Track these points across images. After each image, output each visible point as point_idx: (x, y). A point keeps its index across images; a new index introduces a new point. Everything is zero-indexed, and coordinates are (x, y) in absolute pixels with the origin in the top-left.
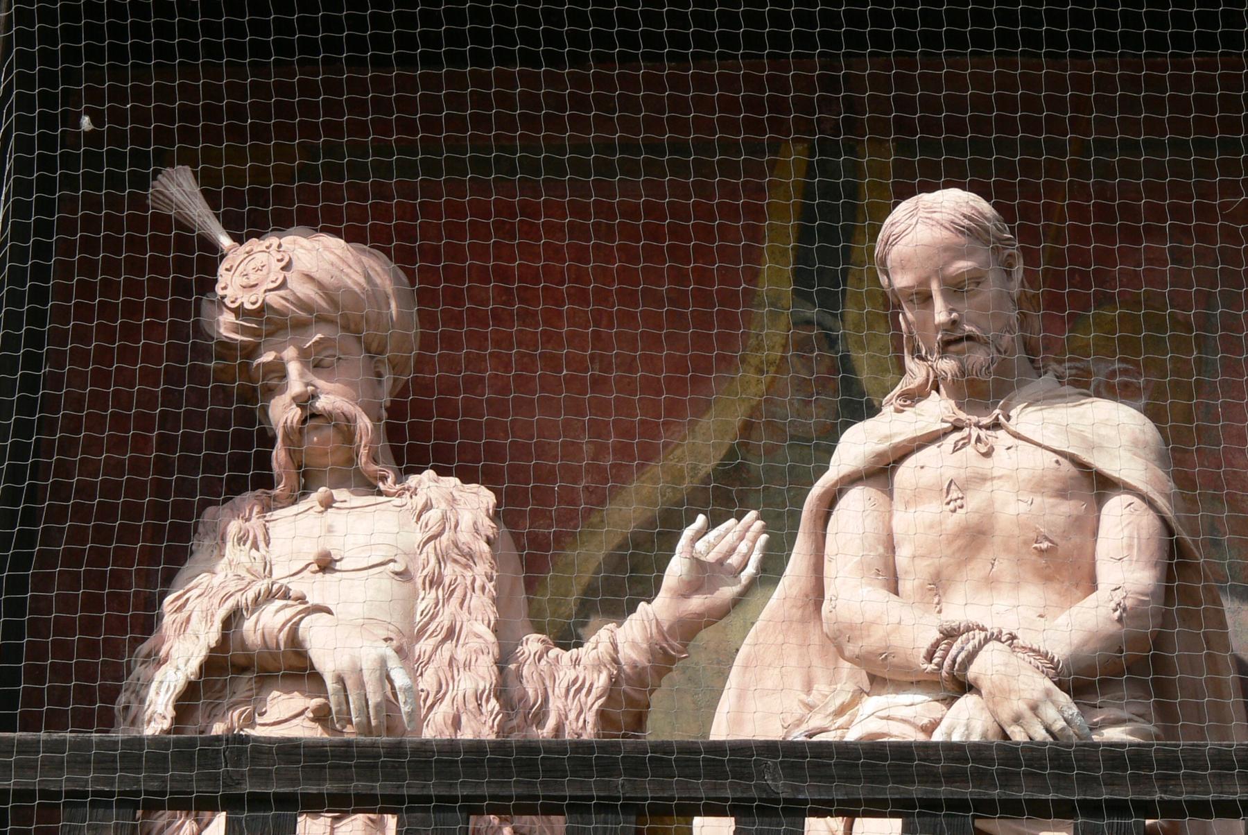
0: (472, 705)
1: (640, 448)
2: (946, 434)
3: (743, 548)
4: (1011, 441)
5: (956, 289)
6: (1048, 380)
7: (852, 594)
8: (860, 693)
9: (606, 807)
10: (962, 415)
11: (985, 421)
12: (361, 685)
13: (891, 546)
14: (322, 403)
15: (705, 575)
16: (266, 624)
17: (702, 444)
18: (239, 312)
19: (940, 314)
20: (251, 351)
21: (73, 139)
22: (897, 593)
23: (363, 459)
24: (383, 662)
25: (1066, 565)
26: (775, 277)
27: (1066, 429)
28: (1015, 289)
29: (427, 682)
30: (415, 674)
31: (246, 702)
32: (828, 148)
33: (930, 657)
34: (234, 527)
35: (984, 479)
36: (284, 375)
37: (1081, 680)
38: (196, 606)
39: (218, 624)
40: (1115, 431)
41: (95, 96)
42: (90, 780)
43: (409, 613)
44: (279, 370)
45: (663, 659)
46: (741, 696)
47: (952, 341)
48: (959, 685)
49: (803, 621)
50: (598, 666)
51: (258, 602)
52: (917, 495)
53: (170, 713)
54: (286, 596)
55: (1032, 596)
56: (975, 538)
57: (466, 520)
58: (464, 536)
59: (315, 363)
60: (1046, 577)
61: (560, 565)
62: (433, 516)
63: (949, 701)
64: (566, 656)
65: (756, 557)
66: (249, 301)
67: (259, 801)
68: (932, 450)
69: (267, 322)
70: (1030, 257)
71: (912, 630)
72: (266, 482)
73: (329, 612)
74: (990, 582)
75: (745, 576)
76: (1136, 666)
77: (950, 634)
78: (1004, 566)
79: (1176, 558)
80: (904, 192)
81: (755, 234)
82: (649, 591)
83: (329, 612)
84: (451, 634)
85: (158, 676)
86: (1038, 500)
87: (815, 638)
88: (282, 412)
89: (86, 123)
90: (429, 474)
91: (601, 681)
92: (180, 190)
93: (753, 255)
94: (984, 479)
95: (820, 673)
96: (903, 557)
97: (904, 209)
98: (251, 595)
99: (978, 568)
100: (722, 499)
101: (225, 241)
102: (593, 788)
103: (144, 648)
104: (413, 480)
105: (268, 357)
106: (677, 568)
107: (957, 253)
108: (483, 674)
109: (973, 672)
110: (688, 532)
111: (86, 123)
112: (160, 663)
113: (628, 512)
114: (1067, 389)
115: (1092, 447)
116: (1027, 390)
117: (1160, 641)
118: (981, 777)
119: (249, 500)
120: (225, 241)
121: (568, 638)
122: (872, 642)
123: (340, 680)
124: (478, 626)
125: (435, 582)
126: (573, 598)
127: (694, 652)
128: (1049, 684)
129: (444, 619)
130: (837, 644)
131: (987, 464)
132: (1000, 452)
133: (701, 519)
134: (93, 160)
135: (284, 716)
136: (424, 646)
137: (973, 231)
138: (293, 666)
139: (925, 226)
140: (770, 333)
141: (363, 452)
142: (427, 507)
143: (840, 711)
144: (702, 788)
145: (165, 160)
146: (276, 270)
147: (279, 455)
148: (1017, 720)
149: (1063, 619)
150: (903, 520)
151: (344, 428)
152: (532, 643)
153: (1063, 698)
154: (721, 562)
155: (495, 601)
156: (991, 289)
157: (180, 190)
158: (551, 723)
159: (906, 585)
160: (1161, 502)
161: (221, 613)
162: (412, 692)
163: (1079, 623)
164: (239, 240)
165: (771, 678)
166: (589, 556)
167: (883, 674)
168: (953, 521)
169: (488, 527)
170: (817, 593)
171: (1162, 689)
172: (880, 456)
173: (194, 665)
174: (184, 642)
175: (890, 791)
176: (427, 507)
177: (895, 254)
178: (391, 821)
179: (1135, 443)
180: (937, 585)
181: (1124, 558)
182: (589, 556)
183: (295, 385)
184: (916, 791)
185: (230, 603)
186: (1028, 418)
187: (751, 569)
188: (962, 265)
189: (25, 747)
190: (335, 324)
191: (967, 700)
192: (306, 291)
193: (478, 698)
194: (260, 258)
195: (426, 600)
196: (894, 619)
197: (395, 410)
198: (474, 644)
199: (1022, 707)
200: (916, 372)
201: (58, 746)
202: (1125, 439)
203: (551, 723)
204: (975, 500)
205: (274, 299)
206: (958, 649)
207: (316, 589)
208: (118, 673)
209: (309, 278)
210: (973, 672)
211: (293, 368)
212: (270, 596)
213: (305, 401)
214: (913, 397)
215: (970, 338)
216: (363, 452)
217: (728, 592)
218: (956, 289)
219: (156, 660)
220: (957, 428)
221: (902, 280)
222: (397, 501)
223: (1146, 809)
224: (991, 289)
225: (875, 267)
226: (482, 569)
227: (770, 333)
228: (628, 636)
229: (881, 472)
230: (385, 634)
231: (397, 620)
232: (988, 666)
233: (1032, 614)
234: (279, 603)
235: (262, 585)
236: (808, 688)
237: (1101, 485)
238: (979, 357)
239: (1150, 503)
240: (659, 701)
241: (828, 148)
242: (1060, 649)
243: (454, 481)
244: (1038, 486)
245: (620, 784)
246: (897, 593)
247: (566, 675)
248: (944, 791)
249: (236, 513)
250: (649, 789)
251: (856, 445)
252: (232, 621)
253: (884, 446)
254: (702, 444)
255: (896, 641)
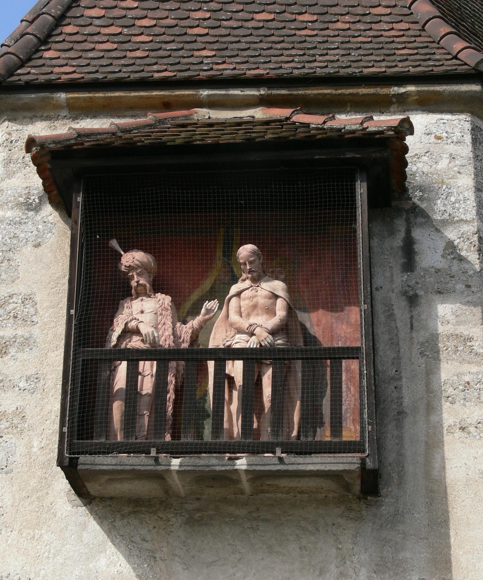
0: (168, 337)
1: (196, 285)
2: (249, 288)
3: (215, 306)
4: (261, 289)
5: (251, 263)
6: (267, 277)
7: (234, 317)
8: (235, 334)
9: (192, 359)
10: (252, 284)
11: (256, 285)
12: (149, 336)
13: (240, 308)
14: (141, 282)
15: (208, 311)
16: (133, 324)
17: (207, 284)
18: (125, 266)
19: (248, 268)
20: (128, 273)
21: (95, 240)
22: (241, 317)
23: (148, 292)
24: (153, 332)
25: (271, 311)
26: (219, 253)
27: (270, 287)
28: (261, 261)
29: (160, 333)
30: (158, 332)
31: (130, 337)
32: (228, 228)
33: (247, 329)
34: (126, 305)
35: (256, 296)
36: (134, 277)
37: (273, 333)
38: (120, 321)
39: (124, 325)
40: (278, 286)
41: (99, 232)
42: (103, 357)
43: (157, 321)
44: (133, 276)
45: (201, 327)
46: (215, 333)
47: (250, 272)
48: (252, 334)
49: (225, 320)
50: (190, 328)
51: (131, 321)
52: (244, 299)
53: (116, 341)
54: (136, 319)
55: (265, 317)
56: (255, 307)
57: (166, 303)
58: (166, 306)
59: (139, 275)
60: (267, 313)
61: (183, 311)
62: (161, 302)
63: (251, 336)
64: (185, 326)
65: (217, 307)
66: (127, 264)
67: (132, 360)
68: (247, 291)
69: (130, 268)
70: (263, 255)
71: (244, 324)
72: (132, 296)
73: (143, 322)
74: (258, 315)
75: (215, 311)
76: (282, 329)
77: (251, 326)
78: (260, 311)
79: (290, 310)
80: (242, 244)
81: (215, 244)
82: (198, 313)
83: (143, 322)
84: (164, 324)
85: (114, 334)
86: (266, 300)
87: (227, 323)
88: (134, 284)
89: (98, 236)
90: (159, 294)
91: (191, 331)
92: (114, 243)
93: (215, 248)
94: (256, 296)
95: (228, 329)
96: (242, 309)
97: (241, 248)
98: (129, 319)
99: (255, 312)
100: (210, 296)
101: (122, 253)
102: (190, 356)
103: (111, 328)
104: (157, 295)
105: (131, 274)
106: (203, 311)
107: (251, 257)
108: (169, 332)
109: (255, 332)
110: (205, 304)
111: (98, 236)
112: (115, 331)
113: (195, 296)
114: (270, 279)
115: (275, 290)
116: (263, 280)
117: (287, 325)
118: (256, 354)
119: (128, 299)
120: (122, 253)
121: (185, 322)
122: (237, 326)
123: (145, 335)
124: (169, 323)
125: (161, 314)
126: (186, 311)
127: (207, 326)
128: (268, 334)
129: (163, 321)
130: (231, 325)
131: (256, 293)
132: (259, 291)
133: (207, 301)
134: (99, 244)
135: (135, 343)
136: (160, 326)
137: (254, 253)
138: (137, 332)
139: (246, 251)
140: (219, 263)
141: (148, 291)
142: (159, 301)
143: (232, 337)
144: (208, 356)
145: (112, 238)
146: (132, 258)
147: (133, 291)
148: (263, 341)
149: (270, 322)
150: (242, 303)
151: (145, 286)
152: (178, 324)
153: (270, 336)
154: (211, 309)
155: (172, 317)
156: (257, 262)
157: (114, 243)
158: (182, 339)
159: (243, 315)
160: (287, 299)
161: (124, 323)
162: (158, 336)
163: (272, 322)
164: (125, 252)
165: (220, 329)
166: (188, 305)
167: (240, 331)
168: (251, 304)
169: (170, 304)
170: (227, 316)
171: (287, 334)
172: (238, 292)
173: (120, 332)
174: (118, 330)
175: (241, 357)
176: (159, 301)
177: (240, 256)
178: (155, 362)
179: (283, 288)
180: (249, 315)
181: (281, 312)
182: (188, 305)
183: (136, 279)
184: (245, 356)
185: (126, 321)
186: (264, 285)
187: (216, 310)
188: (252, 259)
189: (92, 351)
190: (143, 268)
191: (254, 337)
192: (137, 263)
193: (169, 335)
194: (129, 256)
195: (160, 318)
196: (241, 322)
197: (154, 281)
198: (169, 326)
199: (263, 338)
200: (244, 276)
201: (97, 351)
202: (280, 288)
203: (182, 339)
204: (255, 300)
205: (132, 264)
206: (252, 328)
207: (140, 317)
208: (107, 333)
209: (138, 260)
210: (255, 332)
211: (135, 276)
212: (133, 319)
213: (138, 282)
214: (244, 280)
215: (253, 271)
216: (148, 291)
217: (212, 314)
218: (251, 263)
219: (113, 331)
220: (251, 287)
221: (241, 261)
222: (154, 299)
223: (284, 359)
224: (257, 262)
225: (236, 258)
226: (169, 312)
227: (219, 263)
228: (195, 322)
229: (238, 294)
230: (152, 325)
231: (155, 322)
232: (258, 331)
233: (265, 320)
234: (134, 321)
235: (131, 318)
236: (227, 331)
237: (277, 297)
238: (255, 274)
239: (285, 300)
240: (200, 335)
241: (228, 228)
242: (269, 328)
243: (164, 295)
244: (266, 297)
245: (195, 356)
246: (241, 317)
247: (184, 330)
248: (250, 356)
249: (126, 302)
250: (199, 356)
251: (234, 289)
252: (126, 324)
253: (239, 290)
254: (207, 284)
255: (241, 326)
